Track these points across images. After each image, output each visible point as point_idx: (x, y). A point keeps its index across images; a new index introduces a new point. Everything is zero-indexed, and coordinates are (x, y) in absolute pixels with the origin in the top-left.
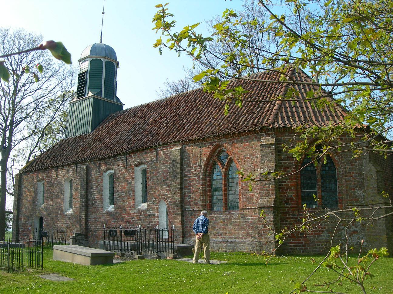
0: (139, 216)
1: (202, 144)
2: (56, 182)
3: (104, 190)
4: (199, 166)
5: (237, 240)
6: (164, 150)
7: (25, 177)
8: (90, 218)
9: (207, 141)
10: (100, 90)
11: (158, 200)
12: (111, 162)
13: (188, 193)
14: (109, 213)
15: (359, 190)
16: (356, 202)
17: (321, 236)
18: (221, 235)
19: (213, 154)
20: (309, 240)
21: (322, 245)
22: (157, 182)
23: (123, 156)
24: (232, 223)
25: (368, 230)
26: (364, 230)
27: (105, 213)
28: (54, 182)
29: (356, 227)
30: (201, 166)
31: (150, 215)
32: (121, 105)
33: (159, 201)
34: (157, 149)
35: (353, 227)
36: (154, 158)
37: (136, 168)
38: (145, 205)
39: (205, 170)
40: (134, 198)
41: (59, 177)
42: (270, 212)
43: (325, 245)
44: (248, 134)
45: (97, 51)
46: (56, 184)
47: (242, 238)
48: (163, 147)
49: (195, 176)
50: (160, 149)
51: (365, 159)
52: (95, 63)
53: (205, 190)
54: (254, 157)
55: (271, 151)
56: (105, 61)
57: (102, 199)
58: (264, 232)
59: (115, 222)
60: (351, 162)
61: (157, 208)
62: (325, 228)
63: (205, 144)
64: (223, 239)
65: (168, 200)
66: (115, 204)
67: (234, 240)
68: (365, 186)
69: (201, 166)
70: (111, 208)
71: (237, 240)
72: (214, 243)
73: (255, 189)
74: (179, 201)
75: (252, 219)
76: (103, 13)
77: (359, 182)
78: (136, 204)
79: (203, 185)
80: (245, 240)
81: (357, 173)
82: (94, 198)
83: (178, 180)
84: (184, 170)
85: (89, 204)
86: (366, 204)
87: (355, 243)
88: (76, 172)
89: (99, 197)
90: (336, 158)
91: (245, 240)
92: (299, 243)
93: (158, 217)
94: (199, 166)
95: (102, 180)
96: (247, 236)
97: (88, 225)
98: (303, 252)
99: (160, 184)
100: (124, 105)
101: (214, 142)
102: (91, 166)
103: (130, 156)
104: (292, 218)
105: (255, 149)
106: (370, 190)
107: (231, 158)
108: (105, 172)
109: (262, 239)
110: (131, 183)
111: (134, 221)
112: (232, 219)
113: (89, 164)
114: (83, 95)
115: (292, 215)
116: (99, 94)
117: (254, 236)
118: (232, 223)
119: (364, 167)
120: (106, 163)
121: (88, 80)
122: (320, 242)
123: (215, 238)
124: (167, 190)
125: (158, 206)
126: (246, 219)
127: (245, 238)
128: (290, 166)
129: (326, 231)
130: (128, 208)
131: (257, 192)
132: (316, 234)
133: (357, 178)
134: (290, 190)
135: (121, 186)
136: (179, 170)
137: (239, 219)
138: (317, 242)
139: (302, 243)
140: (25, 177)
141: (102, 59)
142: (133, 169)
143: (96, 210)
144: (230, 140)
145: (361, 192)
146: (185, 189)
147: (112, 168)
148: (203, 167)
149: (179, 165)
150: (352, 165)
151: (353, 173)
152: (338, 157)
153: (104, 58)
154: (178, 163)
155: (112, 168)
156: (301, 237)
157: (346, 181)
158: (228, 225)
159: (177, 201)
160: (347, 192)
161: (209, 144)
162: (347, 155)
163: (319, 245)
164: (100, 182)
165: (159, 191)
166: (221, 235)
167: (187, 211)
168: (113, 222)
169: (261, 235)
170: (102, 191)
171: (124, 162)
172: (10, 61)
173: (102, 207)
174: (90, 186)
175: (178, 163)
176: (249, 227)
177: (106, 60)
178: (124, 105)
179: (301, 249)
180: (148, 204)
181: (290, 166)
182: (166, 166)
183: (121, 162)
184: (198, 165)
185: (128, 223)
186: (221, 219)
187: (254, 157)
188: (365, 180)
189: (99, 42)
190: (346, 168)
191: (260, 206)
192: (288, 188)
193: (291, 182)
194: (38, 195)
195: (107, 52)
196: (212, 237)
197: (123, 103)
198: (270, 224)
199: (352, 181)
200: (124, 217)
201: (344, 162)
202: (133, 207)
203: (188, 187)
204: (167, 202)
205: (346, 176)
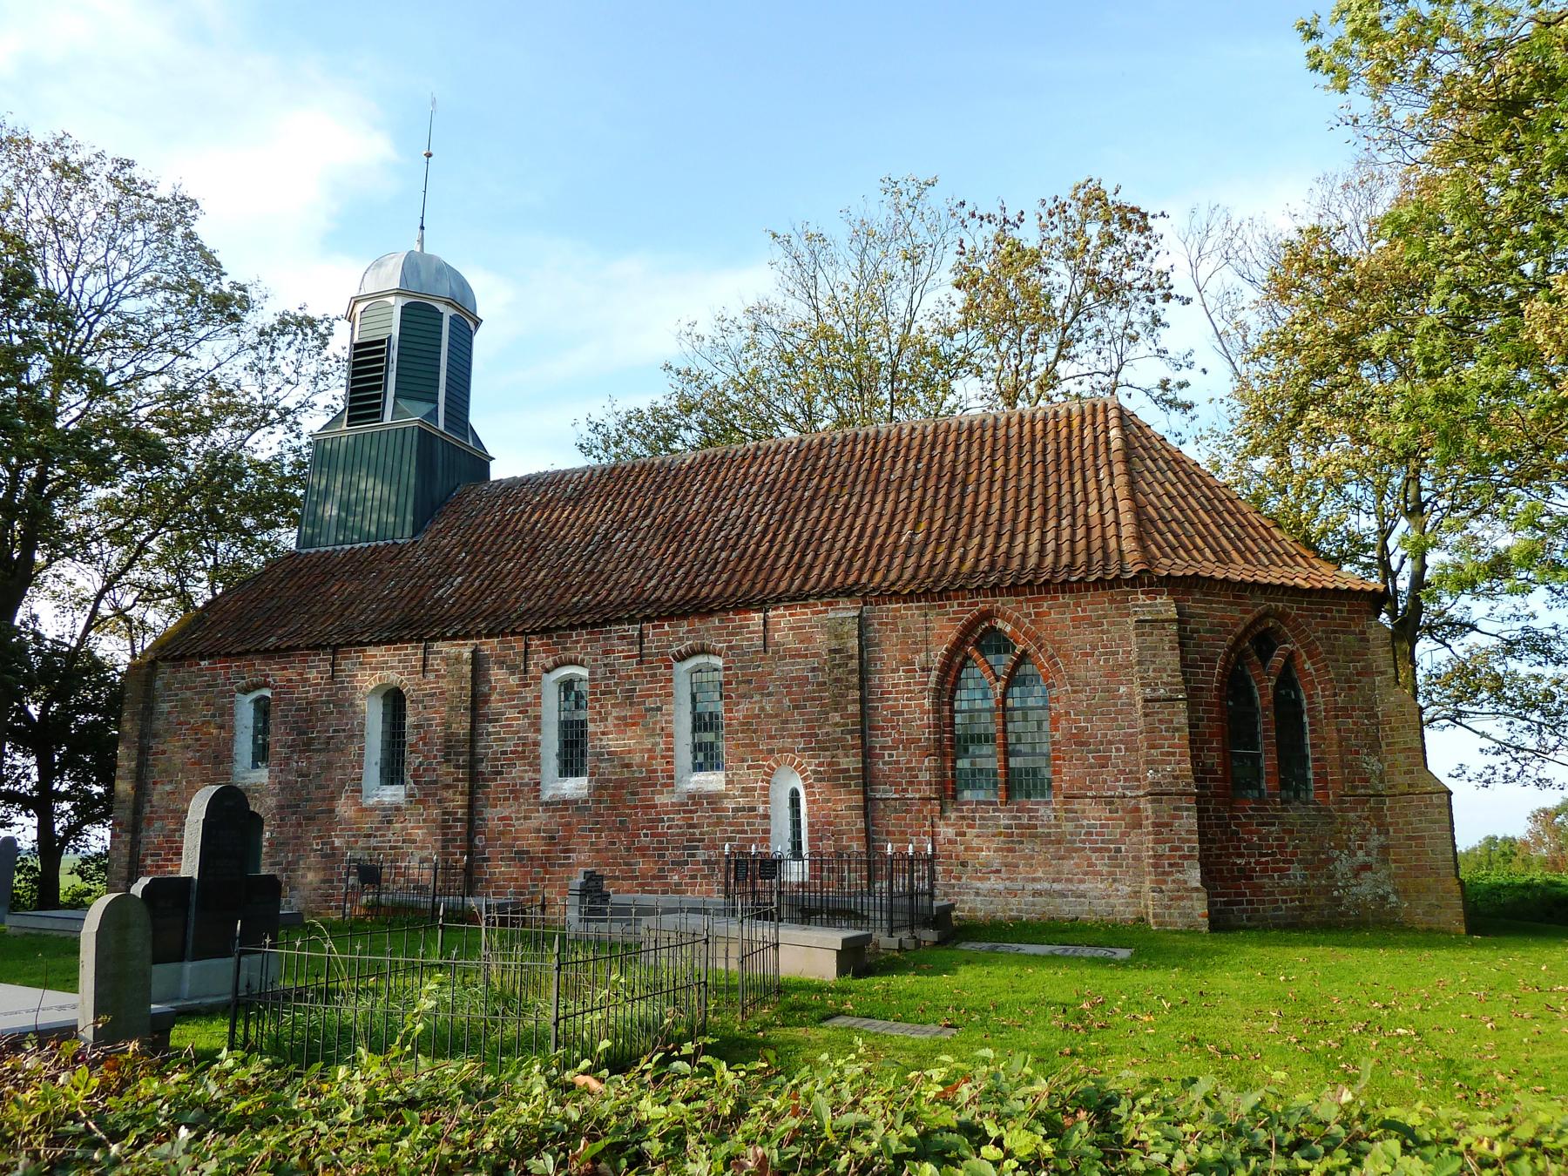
0: (691, 812)
1: (932, 608)
2: (327, 696)
3: (544, 729)
4: (923, 670)
5: (1056, 886)
6: (791, 615)
7: (165, 673)
8: (484, 820)
9: (948, 598)
10: (432, 406)
11: (769, 767)
12: (577, 642)
13: (883, 748)
14: (563, 804)
15: (1367, 755)
16: (1363, 787)
17: (1288, 877)
18: (998, 871)
19: (966, 636)
20: (1262, 887)
21: (1292, 901)
22: (762, 709)
23: (626, 627)
24: (1036, 837)
25: (1395, 861)
26: (1385, 861)
27: (547, 803)
28: (321, 696)
29: (1368, 854)
30: (930, 670)
31: (736, 810)
32: (481, 462)
33: (773, 769)
34: (767, 611)
35: (1360, 853)
36: (751, 639)
37: (676, 665)
38: (713, 781)
39: (941, 681)
40: (672, 757)
41: (343, 682)
42: (1188, 809)
43: (1300, 900)
44: (1087, 590)
45: (423, 275)
46: (328, 702)
47: (1069, 881)
48: (786, 608)
49: (908, 699)
50: (774, 613)
51: (1382, 673)
52: (419, 316)
53: (939, 740)
54: (1106, 654)
55: (1166, 639)
56: (447, 313)
57: (538, 757)
58: (1171, 865)
59: (591, 830)
60: (1348, 681)
61: (763, 788)
62: (1295, 854)
63: (940, 607)
64: (1008, 883)
65: (809, 764)
66: (592, 774)
67: (1046, 885)
68: (1383, 744)
69: (926, 669)
70: (575, 787)
71: (1056, 886)
72: (977, 894)
73: (1110, 743)
74: (855, 770)
75: (1102, 826)
76: (429, 155)
77: (1367, 733)
78: (677, 775)
79: (935, 726)
80: (1082, 887)
81: (1361, 709)
82: (504, 753)
83: (853, 708)
84: (869, 680)
85: (482, 773)
86: (1389, 792)
87: (1369, 897)
88: (424, 666)
89: (524, 752)
90: (1306, 666)
91: (1082, 887)
92: (1237, 895)
93: (766, 817)
94: (923, 670)
95: (539, 697)
96: (1086, 873)
97: (472, 840)
98: (1249, 919)
99: (776, 716)
100: (493, 459)
101: (970, 605)
102: (490, 646)
103: (654, 627)
104: (1218, 826)
105: (1108, 632)
106: (1401, 757)
107: (1024, 652)
108: (548, 671)
109: (1165, 882)
110: (659, 709)
111: (669, 828)
112: (1035, 827)
113: (481, 644)
114: (377, 415)
115: (1217, 818)
116: (433, 415)
117: (1110, 873)
118: (1036, 836)
119: (1380, 695)
120: (555, 643)
121: (393, 366)
122: (1287, 893)
123: (980, 879)
124: (802, 735)
125: (768, 782)
126: (1082, 826)
127: (1081, 881)
128: (1206, 682)
129: (1300, 862)
130: (644, 786)
131: (1118, 750)
132: (1274, 870)
133: (1363, 724)
134: (1209, 750)
135: (617, 718)
136: (855, 679)
137: (1058, 826)
138: (1281, 894)
139: (1244, 894)
140: (165, 673)
141: (441, 307)
142: (670, 667)
143: (511, 792)
144: (1028, 600)
145: (1374, 760)
146: (871, 736)
147: (583, 660)
148: (934, 673)
149: (854, 664)
150: (1351, 688)
151: (1354, 709)
152: (1313, 664)
153: (448, 304)
154: (851, 657)
155: (583, 660)
156: (1240, 878)
157: (1339, 731)
158: (1022, 843)
159: (847, 770)
160: (1342, 761)
161: (956, 608)
162: (1337, 661)
163: (1285, 901)
164: (529, 705)
165: (771, 737)
166: (998, 871)
167: (881, 799)
168: (583, 830)
169: (1164, 873)
170: (538, 731)
171: (632, 643)
172: (914, 307)
173: (538, 784)
174: (485, 715)
175: (851, 657)
176: (1095, 850)
177: (452, 312)
178: (493, 459)
179: (1245, 911)
180: (727, 775)
181: (1206, 682)
182: (799, 664)
183: (621, 647)
184: (917, 667)
185: (646, 835)
186: (997, 826)
187: (1106, 654)
188: (1383, 729)
189: (418, 250)
190: (1335, 695)
191: (1158, 789)
192: (1206, 742)
193: (1209, 727)
194: (237, 738)
195: (454, 286)
196: (968, 878)
197: (491, 454)
198: (1189, 841)
199: (1351, 731)
200: (629, 815)
201: (1331, 680)
202: (665, 785)
203: (882, 728)
204: (801, 773)
205: (1337, 717)
